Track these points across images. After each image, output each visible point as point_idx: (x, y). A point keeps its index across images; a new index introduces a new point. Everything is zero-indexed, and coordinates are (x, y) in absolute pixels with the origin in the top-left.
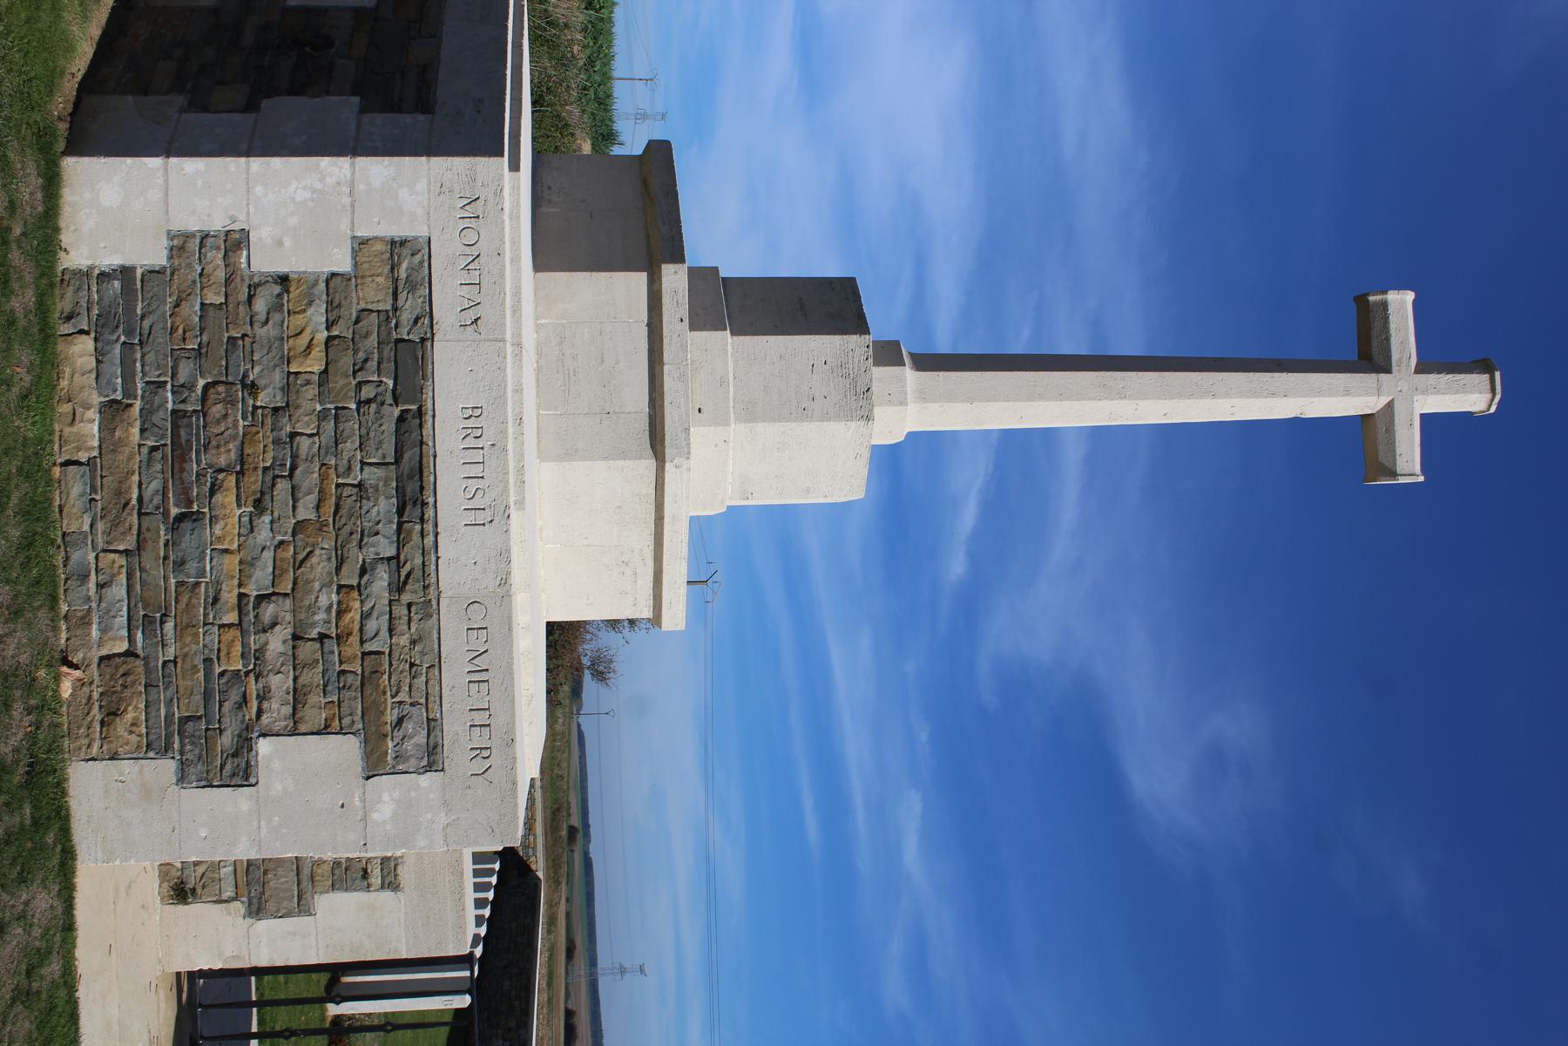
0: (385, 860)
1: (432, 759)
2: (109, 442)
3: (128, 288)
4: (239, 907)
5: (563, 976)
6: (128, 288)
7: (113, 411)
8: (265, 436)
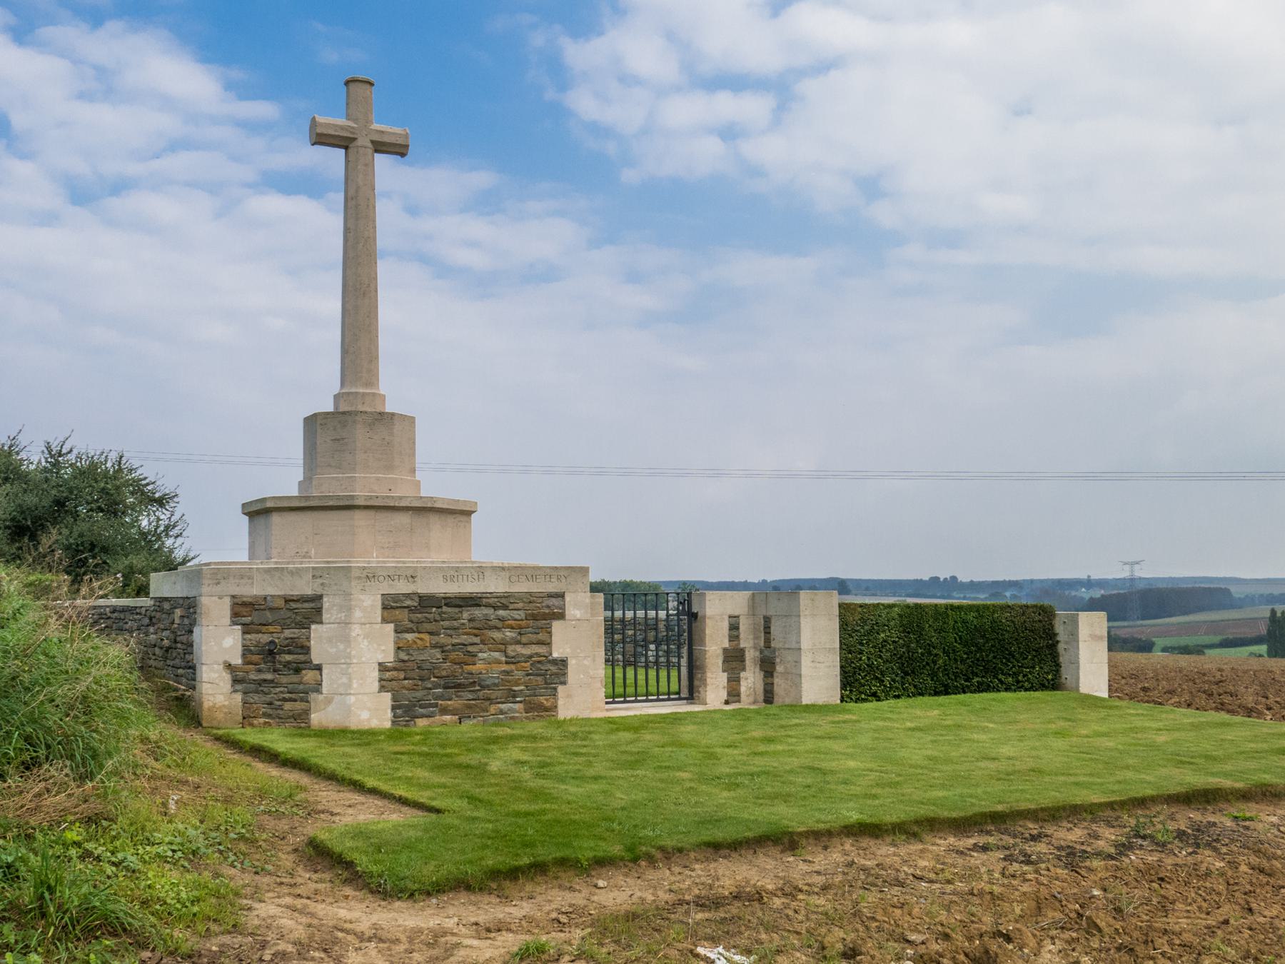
1: (561, 596)
7: (444, 711)
8: (453, 656)
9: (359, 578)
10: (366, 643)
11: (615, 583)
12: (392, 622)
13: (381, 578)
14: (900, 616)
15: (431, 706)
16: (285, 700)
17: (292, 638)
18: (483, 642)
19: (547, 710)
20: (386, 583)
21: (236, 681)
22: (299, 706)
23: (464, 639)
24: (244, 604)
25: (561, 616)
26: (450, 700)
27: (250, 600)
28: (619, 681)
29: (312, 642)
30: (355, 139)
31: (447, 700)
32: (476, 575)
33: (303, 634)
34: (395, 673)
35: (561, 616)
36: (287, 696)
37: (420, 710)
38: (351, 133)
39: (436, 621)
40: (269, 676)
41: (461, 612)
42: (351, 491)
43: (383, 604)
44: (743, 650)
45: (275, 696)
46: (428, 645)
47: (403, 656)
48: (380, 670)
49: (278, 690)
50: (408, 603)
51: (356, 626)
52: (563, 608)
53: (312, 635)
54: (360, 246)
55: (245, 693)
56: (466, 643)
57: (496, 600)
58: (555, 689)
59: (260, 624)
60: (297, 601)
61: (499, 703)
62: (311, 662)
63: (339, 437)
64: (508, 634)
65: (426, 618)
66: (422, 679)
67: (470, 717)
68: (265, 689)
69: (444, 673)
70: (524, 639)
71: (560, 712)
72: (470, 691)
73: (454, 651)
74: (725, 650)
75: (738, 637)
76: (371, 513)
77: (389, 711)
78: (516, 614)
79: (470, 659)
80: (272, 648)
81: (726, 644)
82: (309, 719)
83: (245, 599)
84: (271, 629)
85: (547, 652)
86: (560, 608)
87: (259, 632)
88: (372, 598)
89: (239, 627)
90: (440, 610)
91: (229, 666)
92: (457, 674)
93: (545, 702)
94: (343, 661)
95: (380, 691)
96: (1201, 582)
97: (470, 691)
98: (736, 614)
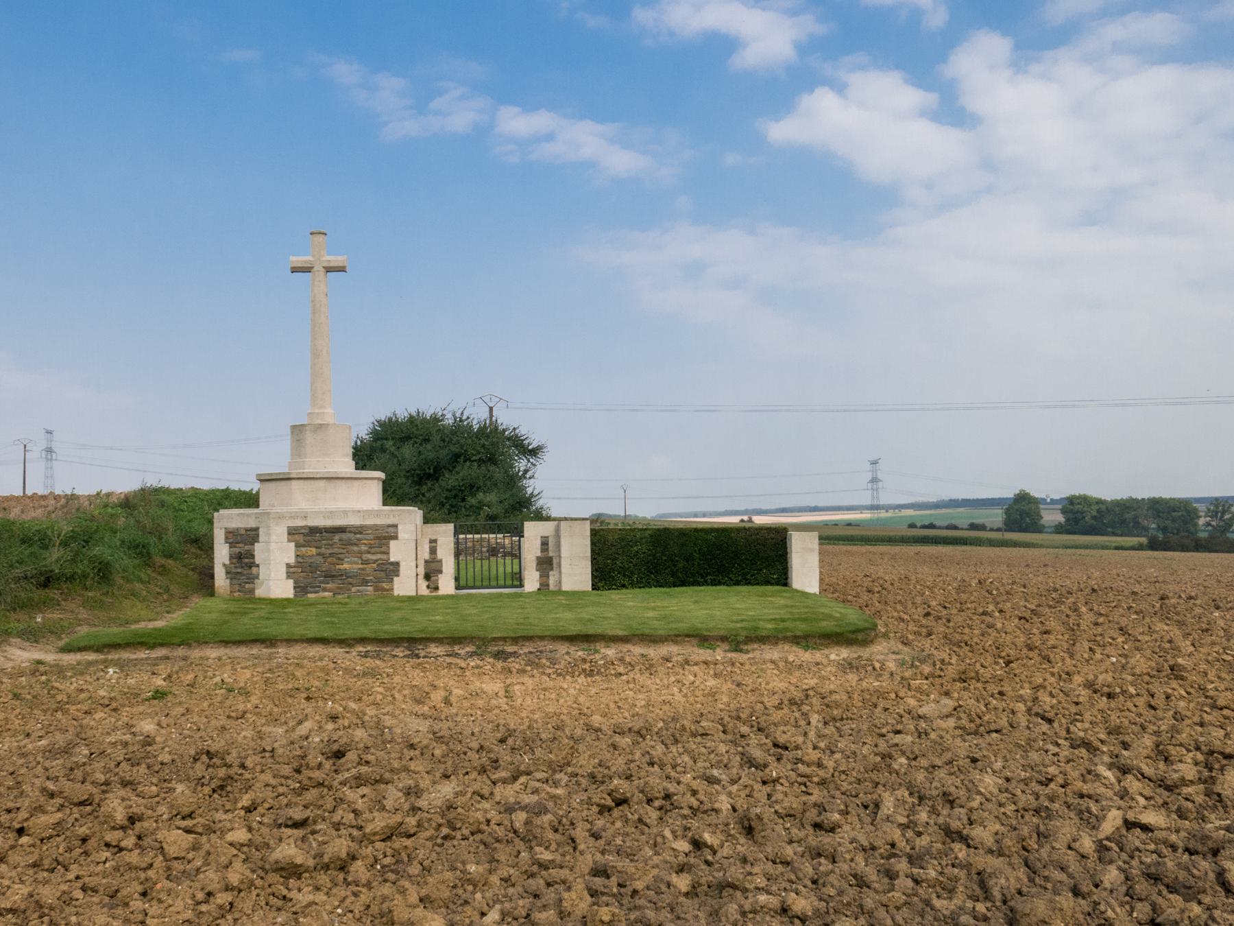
0: (430, 542)
1: (396, 526)
2: (329, 591)
3: (298, 587)
4: (440, 576)
5: (358, 506)
6: (298, 587)
7: (325, 590)
8: (329, 560)
9: (273, 518)
11: (1143, 499)
14: (651, 536)
19: (388, 590)
21: (227, 573)
23: (336, 550)
24: (230, 532)
25: (396, 538)
35: (396, 538)
40: (239, 570)
42: (300, 469)
44: (551, 558)
47: (300, 560)
50: (303, 531)
52: (397, 533)
69: (324, 569)
70: (373, 550)
74: (538, 558)
75: (547, 550)
78: (367, 537)
79: (340, 562)
81: (539, 554)
84: (240, 545)
89: (228, 544)
91: (224, 565)
96: (676, 517)
98: (546, 535)
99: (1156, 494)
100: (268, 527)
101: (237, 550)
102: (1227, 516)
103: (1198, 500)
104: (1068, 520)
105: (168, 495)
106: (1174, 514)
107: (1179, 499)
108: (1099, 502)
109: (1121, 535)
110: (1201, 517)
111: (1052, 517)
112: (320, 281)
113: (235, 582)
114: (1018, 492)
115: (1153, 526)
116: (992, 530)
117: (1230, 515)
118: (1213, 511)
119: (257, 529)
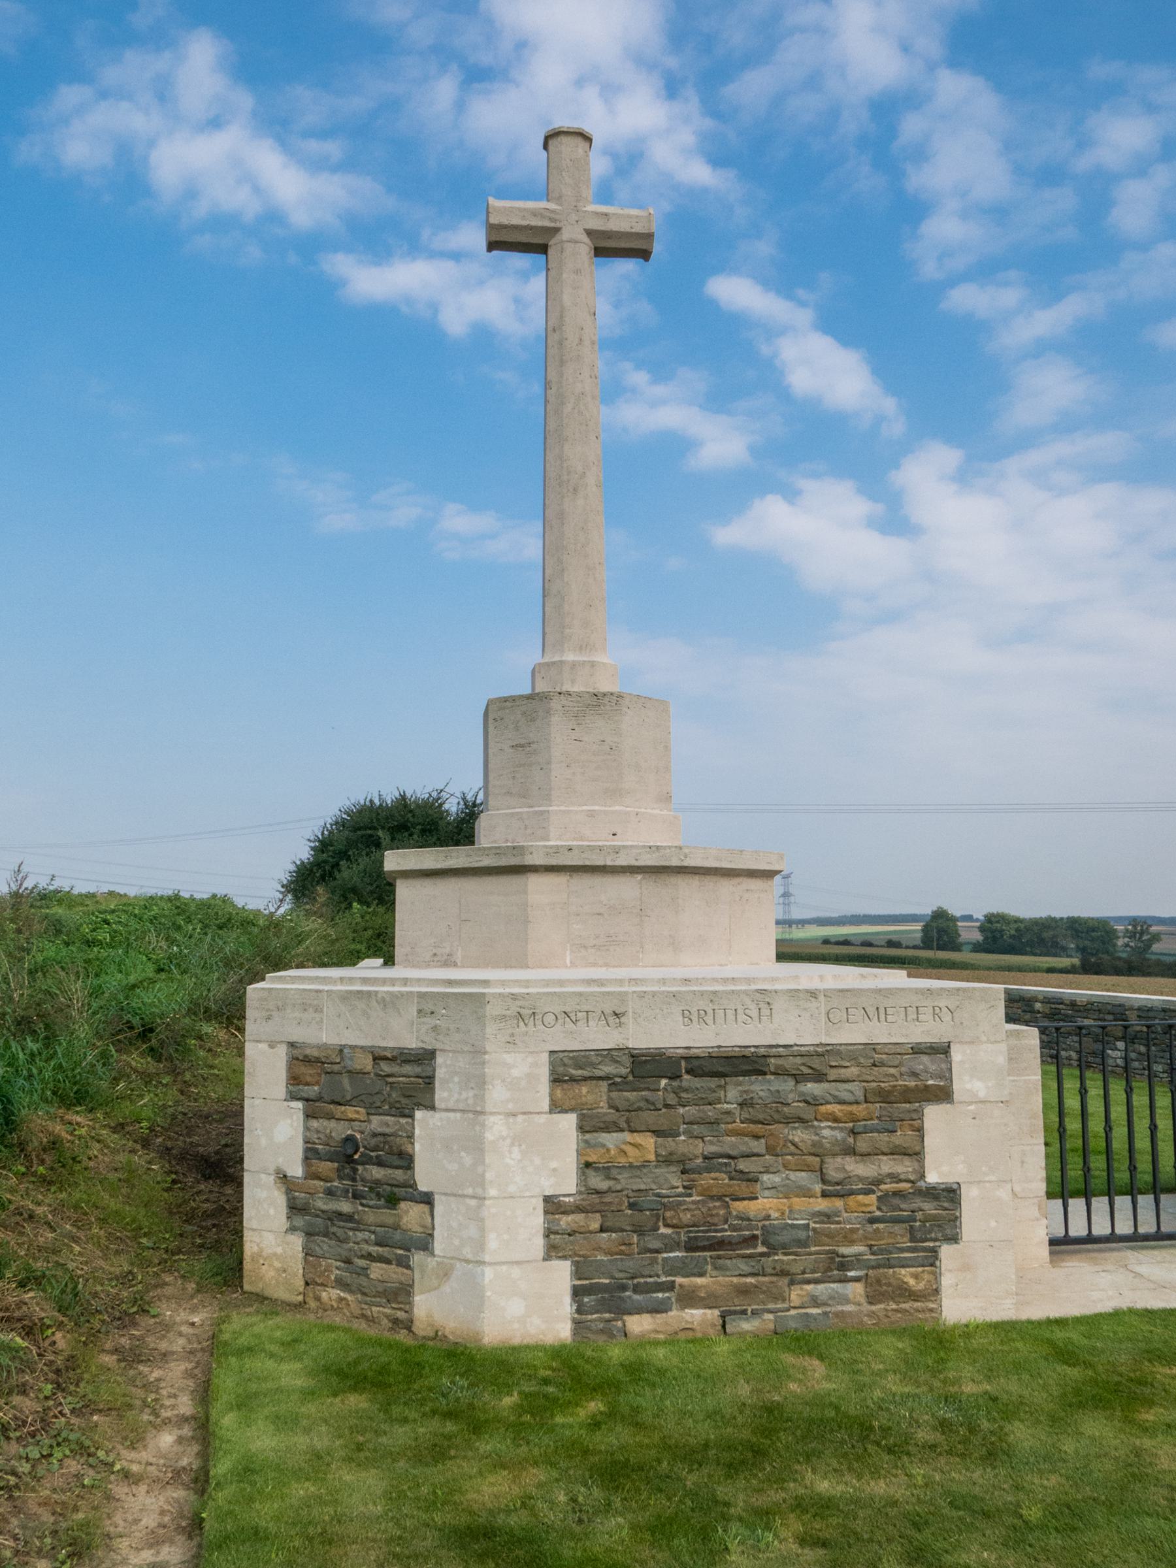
1: (942, 1051)
2: (707, 1301)
7: (689, 1299)
10: (516, 1153)
11: (1062, 919)
12: (572, 1110)
13: (550, 1018)
15: (661, 1287)
16: (369, 1257)
17: (384, 1135)
18: (771, 1150)
19: (914, 1296)
20: (558, 1027)
21: (295, 1209)
22: (393, 1273)
23: (730, 1144)
24: (307, 1060)
25: (943, 1095)
26: (701, 1275)
27: (316, 1053)
28: (1072, 1102)
29: (417, 1146)
30: (557, 230)
31: (694, 1275)
32: (753, 1006)
33: (402, 1128)
34: (579, 1218)
35: (943, 1095)
36: (375, 1250)
37: (637, 1297)
38: (551, 219)
39: (667, 1106)
40: (345, 1207)
41: (723, 1087)
43: (553, 1072)
45: (356, 1247)
46: (652, 1157)
48: (546, 1212)
49: (360, 1235)
50: (607, 1069)
51: (492, 1119)
52: (947, 1075)
53: (417, 1132)
54: (568, 407)
55: (309, 1234)
56: (733, 1153)
57: (799, 1060)
58: (934, 1251)
59: (333, 1102)
60: (393, 1059)
61: (809, 1282)
62: (414, 1186)
63: (523, 741)
64: (826, 1132)
65: (647, 1101)
66: (639, 1231)
67: (744, 1312)
68: (340, 1232)
69: (687, 1217)
70: (863, 1144)
71: (946, 1302)
72: (744, 1257)
73: (709, 1170)
76: (560, 880)
77: (567, 1299)
78: (842, 1091)
79: (741, 1188)
80: (350, 1151)
82: (410, 1303)
83: (308, 1052)
84: (350, 1111)
85: (914, 1171)
86: (941, 1077)
87: (330, 1117)
88: (530, 1059)
89: (299, 1105)
90: (675, 1083)
91: (283, 1178)
92: (715, 1220)
93: (912, 1282)
94: (470, 1191)
95: (547, 1258)
97: (744, 1257)
99: (1075, 913)
100: (478, 1052)
101: (339, 1130)
102: (1145, 937)
103: (1119, 920)
104: (986, 938)
105: (70, 907)
106: (1093, 934)
107: (1098, 919)
108: (1017, 920)
109: (1040, 955)
110: (1119, 937)
111: (970, 934)
112: (577, 272)
113: (324, 1245)
114: (935, 909)
115: (1072, 946)
116: (907, 947)
117: (1149, 936)
118: (1131, 932)
119: (426, 1057)
